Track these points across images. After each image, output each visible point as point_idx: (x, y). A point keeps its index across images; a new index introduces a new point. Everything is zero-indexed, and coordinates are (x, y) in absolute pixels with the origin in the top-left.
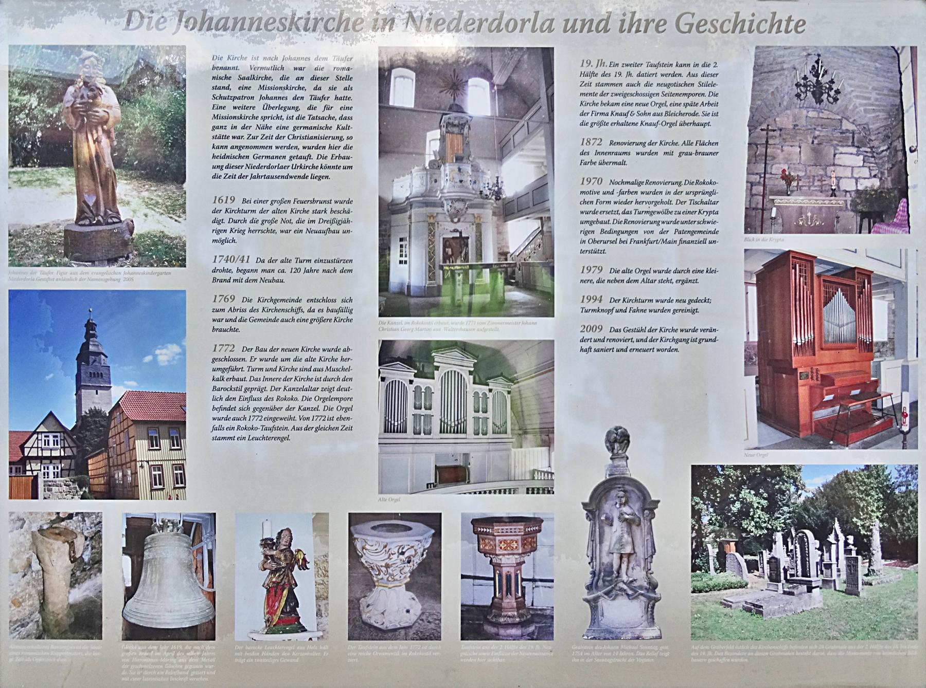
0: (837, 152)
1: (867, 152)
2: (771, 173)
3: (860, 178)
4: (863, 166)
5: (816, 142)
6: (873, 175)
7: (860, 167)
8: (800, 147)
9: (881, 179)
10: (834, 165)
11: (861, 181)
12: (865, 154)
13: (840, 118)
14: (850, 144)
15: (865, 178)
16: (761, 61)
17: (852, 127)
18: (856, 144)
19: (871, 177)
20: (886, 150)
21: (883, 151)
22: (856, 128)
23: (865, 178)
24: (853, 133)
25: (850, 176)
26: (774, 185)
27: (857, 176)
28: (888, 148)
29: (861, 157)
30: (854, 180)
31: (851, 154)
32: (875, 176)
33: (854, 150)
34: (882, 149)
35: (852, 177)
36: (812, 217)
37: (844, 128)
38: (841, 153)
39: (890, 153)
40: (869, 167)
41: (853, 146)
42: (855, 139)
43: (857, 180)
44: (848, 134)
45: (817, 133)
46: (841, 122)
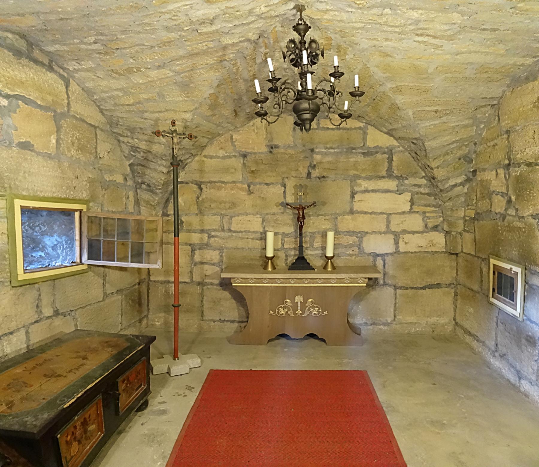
0: (356, 189)
1: (419, 186)
2: (230, 230)
3: (405, 232)
4: (411, 212)
5: (315, 173)
6: (430, 225)
7: (403, 213)
8: (284, 186)
9: (447, 233)
10: (352, 212)
11: (407, 237)
12: (416, 189)
13: (270, 73)
14: (384, 173)
15: (414, 233)
16: (23, 221)
17: (385, 141)
18: (396, 173)
19: (427, 229)
20: (462, 184)
21: (455, 186)
22: (396, 143)
23: (414, 233)
24: (390, 152)
25: (384, 229)
26: (236, 248)
27: (398, 230)
28: (468, 180)
29: (407, 196)
30: (392, 237)
31: (387, 191)
32: (435, 228)
33: (392, 184)
34: (451, 182)
35: (388, 231)
36: (303, 304)
37: (370, 144)
38: (366, 191)
39: (472, 190)
40: (424, 213)
41: (390, 175)
42: (394, 164)
43: (397, 237)
44: (379, 156)
45: (317, 157)
46: (365, 133)
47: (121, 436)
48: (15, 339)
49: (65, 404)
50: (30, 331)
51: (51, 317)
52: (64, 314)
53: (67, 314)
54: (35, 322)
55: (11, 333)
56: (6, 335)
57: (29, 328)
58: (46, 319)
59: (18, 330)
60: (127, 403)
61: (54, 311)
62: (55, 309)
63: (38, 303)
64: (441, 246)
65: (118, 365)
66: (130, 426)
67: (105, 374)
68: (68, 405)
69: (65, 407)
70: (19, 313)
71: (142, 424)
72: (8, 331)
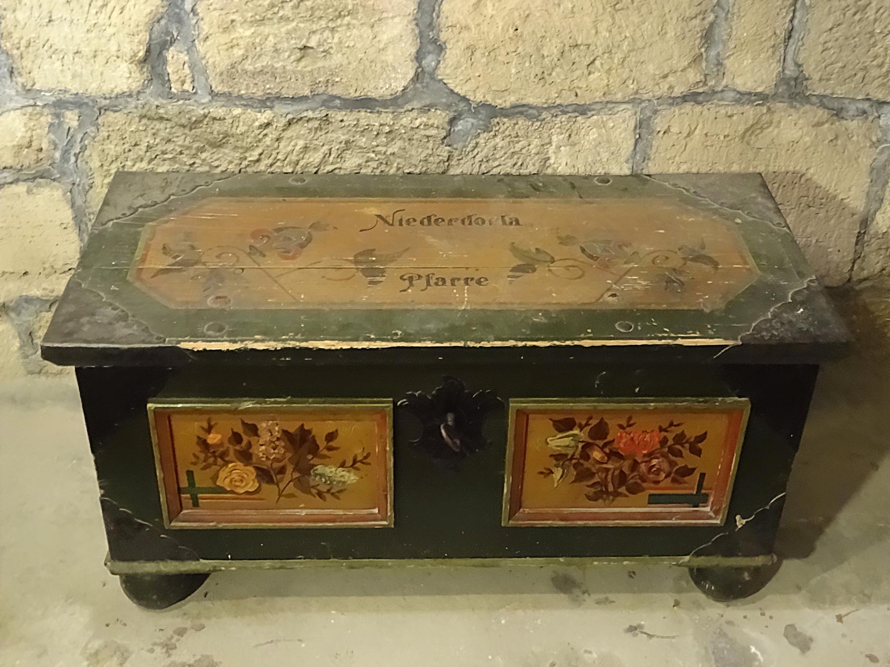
47: (556, 595)
48: (593, 135)
49: (196, 336)
50: (659, 124)
51: (763, 98)
52: (836, 105)
53: (852, 108)
54: (685, 99)
55: (583, 110)
56: (563, 109)
57: (655, 112)
58: (737, 101)
59: (608, 104)
60: (566, 510)
61: (783, 80)
62: (791, 71)
63: (712, 25)
64: (552, 150)
65: (511, 343)
66: (611, 597)
67: (414, 341)
68: (200, 346)
69: (183, 345)
70: (625, 46)
71: (632, 629)
72: (572, 99)
